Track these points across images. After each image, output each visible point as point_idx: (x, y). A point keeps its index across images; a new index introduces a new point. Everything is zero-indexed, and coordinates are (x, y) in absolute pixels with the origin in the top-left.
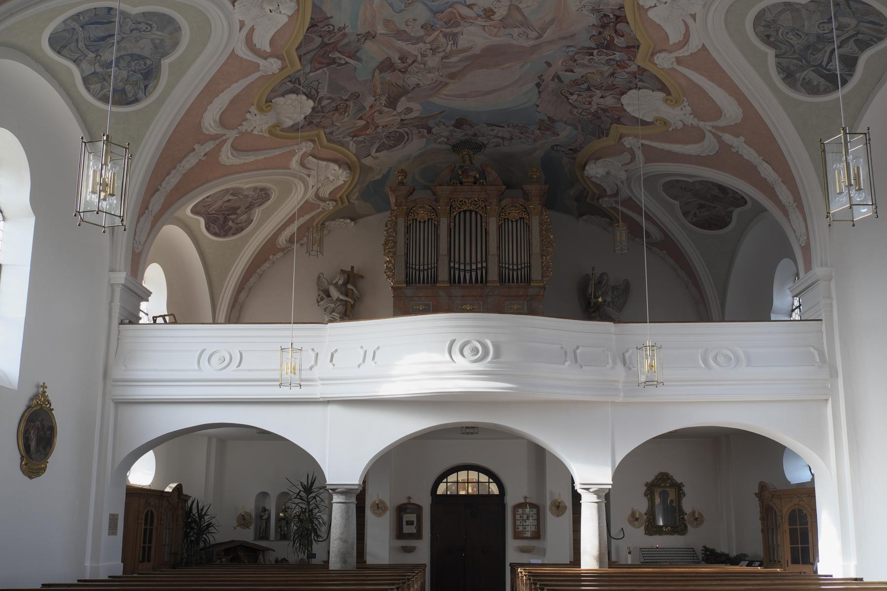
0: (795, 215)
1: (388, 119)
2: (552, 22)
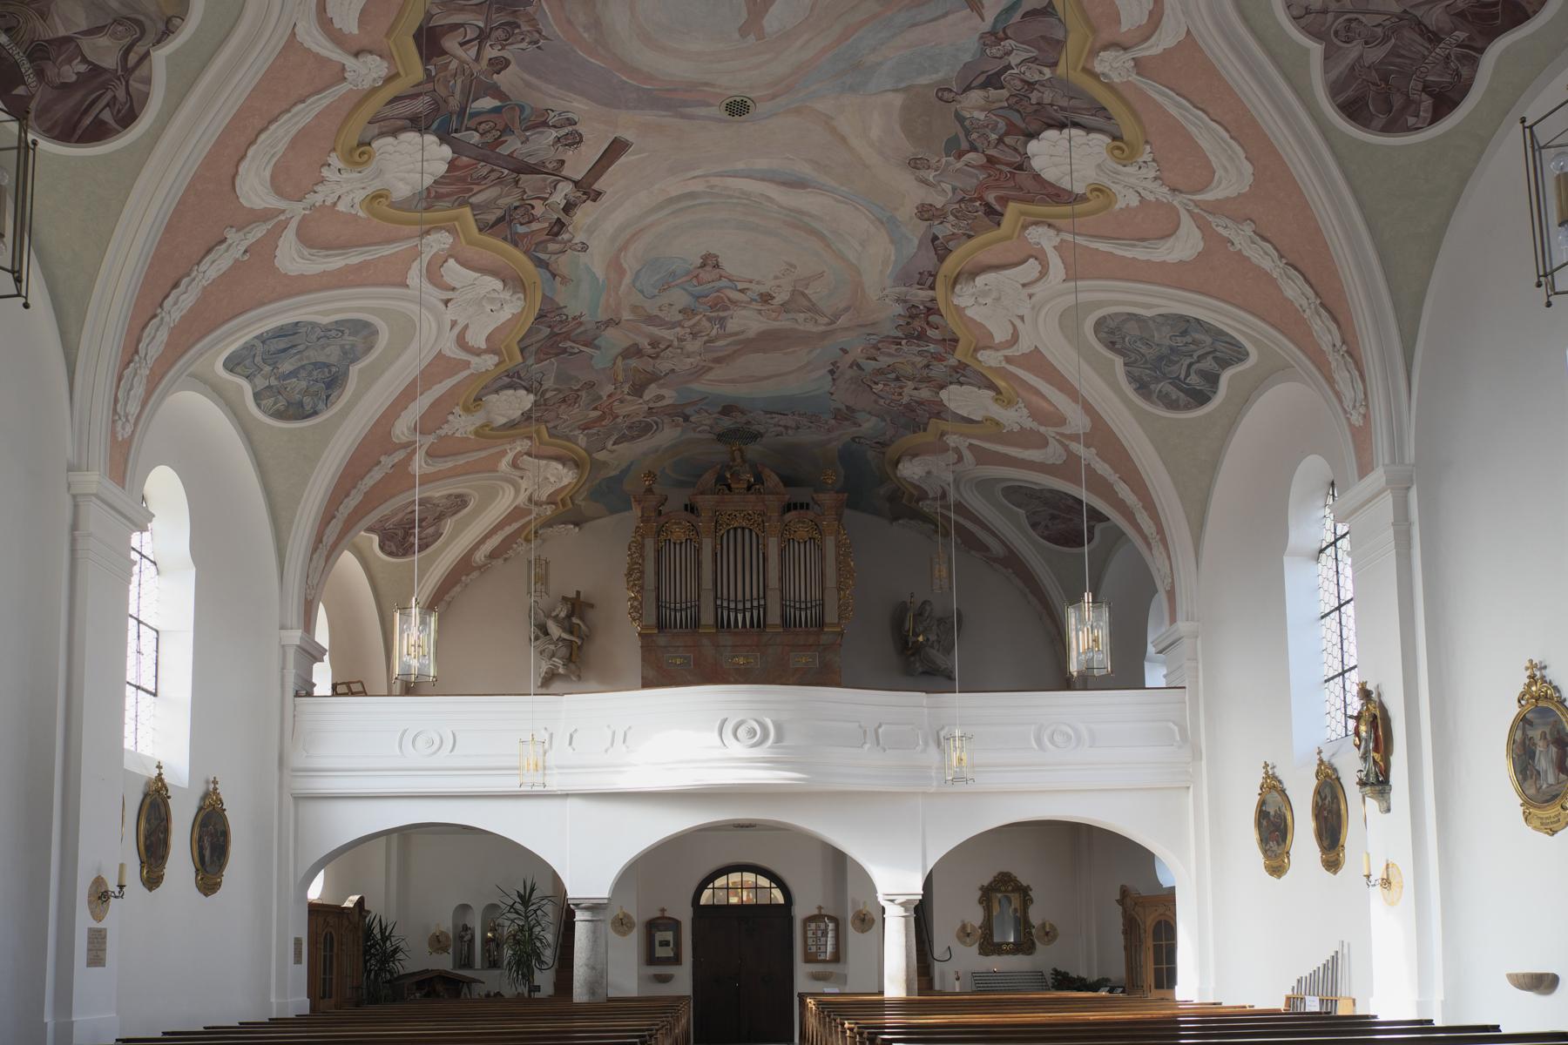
0: (1158, 549)
1: (633, 408)
2: (847, 309)
